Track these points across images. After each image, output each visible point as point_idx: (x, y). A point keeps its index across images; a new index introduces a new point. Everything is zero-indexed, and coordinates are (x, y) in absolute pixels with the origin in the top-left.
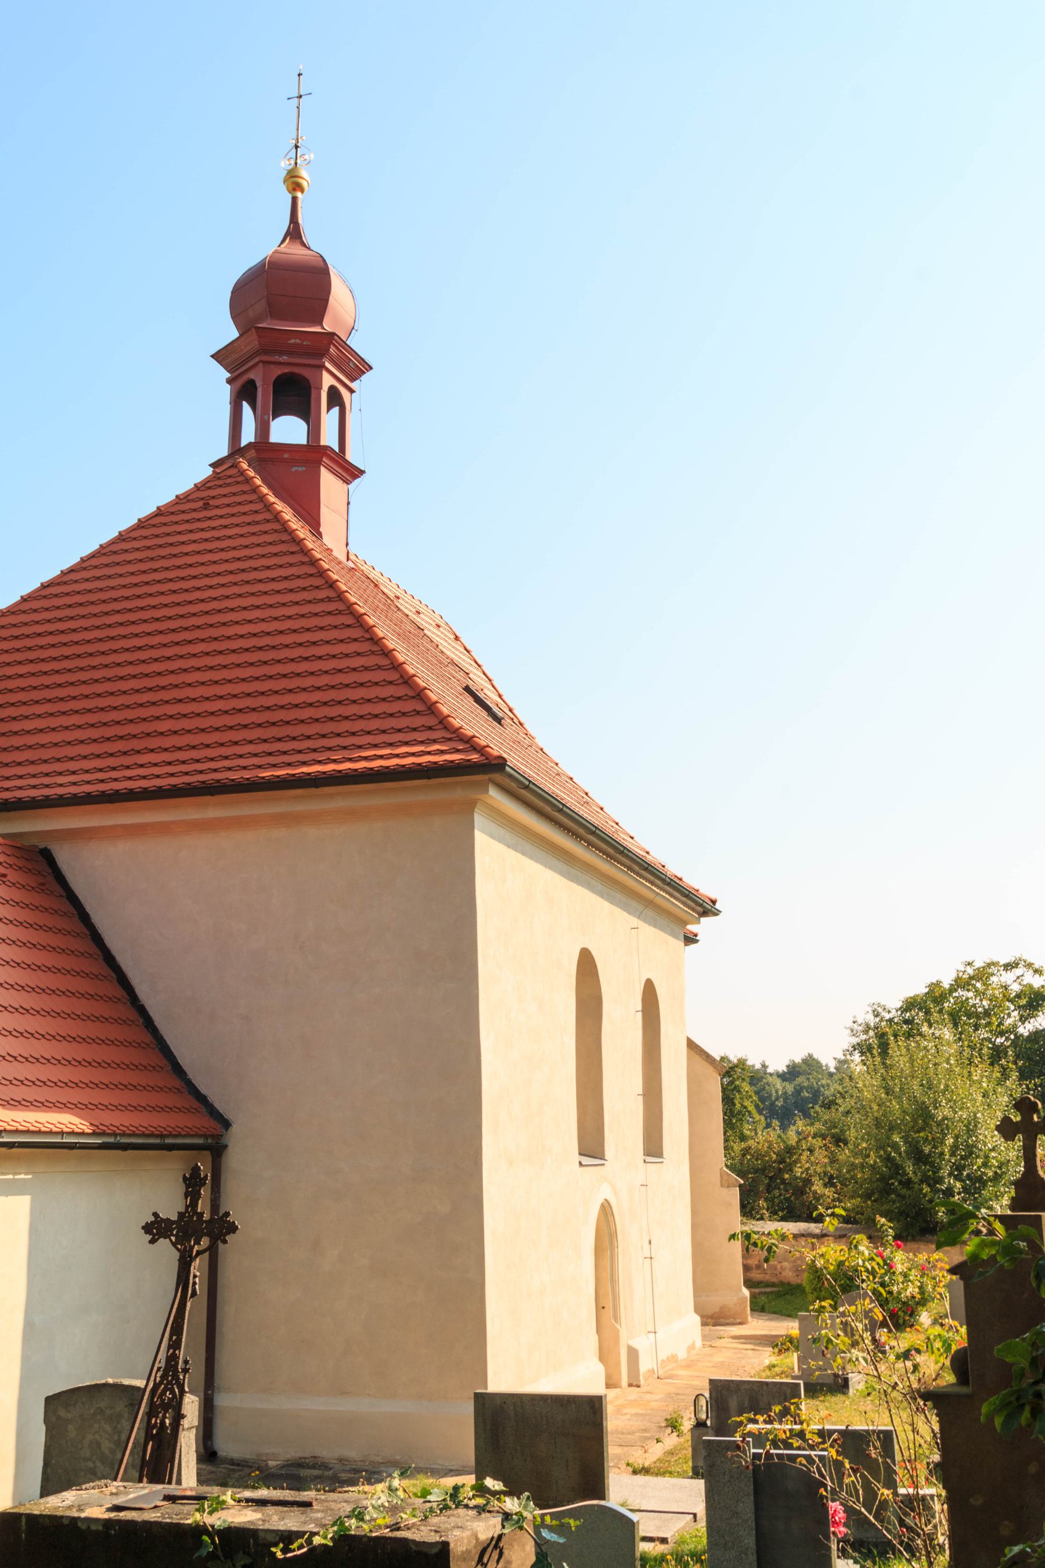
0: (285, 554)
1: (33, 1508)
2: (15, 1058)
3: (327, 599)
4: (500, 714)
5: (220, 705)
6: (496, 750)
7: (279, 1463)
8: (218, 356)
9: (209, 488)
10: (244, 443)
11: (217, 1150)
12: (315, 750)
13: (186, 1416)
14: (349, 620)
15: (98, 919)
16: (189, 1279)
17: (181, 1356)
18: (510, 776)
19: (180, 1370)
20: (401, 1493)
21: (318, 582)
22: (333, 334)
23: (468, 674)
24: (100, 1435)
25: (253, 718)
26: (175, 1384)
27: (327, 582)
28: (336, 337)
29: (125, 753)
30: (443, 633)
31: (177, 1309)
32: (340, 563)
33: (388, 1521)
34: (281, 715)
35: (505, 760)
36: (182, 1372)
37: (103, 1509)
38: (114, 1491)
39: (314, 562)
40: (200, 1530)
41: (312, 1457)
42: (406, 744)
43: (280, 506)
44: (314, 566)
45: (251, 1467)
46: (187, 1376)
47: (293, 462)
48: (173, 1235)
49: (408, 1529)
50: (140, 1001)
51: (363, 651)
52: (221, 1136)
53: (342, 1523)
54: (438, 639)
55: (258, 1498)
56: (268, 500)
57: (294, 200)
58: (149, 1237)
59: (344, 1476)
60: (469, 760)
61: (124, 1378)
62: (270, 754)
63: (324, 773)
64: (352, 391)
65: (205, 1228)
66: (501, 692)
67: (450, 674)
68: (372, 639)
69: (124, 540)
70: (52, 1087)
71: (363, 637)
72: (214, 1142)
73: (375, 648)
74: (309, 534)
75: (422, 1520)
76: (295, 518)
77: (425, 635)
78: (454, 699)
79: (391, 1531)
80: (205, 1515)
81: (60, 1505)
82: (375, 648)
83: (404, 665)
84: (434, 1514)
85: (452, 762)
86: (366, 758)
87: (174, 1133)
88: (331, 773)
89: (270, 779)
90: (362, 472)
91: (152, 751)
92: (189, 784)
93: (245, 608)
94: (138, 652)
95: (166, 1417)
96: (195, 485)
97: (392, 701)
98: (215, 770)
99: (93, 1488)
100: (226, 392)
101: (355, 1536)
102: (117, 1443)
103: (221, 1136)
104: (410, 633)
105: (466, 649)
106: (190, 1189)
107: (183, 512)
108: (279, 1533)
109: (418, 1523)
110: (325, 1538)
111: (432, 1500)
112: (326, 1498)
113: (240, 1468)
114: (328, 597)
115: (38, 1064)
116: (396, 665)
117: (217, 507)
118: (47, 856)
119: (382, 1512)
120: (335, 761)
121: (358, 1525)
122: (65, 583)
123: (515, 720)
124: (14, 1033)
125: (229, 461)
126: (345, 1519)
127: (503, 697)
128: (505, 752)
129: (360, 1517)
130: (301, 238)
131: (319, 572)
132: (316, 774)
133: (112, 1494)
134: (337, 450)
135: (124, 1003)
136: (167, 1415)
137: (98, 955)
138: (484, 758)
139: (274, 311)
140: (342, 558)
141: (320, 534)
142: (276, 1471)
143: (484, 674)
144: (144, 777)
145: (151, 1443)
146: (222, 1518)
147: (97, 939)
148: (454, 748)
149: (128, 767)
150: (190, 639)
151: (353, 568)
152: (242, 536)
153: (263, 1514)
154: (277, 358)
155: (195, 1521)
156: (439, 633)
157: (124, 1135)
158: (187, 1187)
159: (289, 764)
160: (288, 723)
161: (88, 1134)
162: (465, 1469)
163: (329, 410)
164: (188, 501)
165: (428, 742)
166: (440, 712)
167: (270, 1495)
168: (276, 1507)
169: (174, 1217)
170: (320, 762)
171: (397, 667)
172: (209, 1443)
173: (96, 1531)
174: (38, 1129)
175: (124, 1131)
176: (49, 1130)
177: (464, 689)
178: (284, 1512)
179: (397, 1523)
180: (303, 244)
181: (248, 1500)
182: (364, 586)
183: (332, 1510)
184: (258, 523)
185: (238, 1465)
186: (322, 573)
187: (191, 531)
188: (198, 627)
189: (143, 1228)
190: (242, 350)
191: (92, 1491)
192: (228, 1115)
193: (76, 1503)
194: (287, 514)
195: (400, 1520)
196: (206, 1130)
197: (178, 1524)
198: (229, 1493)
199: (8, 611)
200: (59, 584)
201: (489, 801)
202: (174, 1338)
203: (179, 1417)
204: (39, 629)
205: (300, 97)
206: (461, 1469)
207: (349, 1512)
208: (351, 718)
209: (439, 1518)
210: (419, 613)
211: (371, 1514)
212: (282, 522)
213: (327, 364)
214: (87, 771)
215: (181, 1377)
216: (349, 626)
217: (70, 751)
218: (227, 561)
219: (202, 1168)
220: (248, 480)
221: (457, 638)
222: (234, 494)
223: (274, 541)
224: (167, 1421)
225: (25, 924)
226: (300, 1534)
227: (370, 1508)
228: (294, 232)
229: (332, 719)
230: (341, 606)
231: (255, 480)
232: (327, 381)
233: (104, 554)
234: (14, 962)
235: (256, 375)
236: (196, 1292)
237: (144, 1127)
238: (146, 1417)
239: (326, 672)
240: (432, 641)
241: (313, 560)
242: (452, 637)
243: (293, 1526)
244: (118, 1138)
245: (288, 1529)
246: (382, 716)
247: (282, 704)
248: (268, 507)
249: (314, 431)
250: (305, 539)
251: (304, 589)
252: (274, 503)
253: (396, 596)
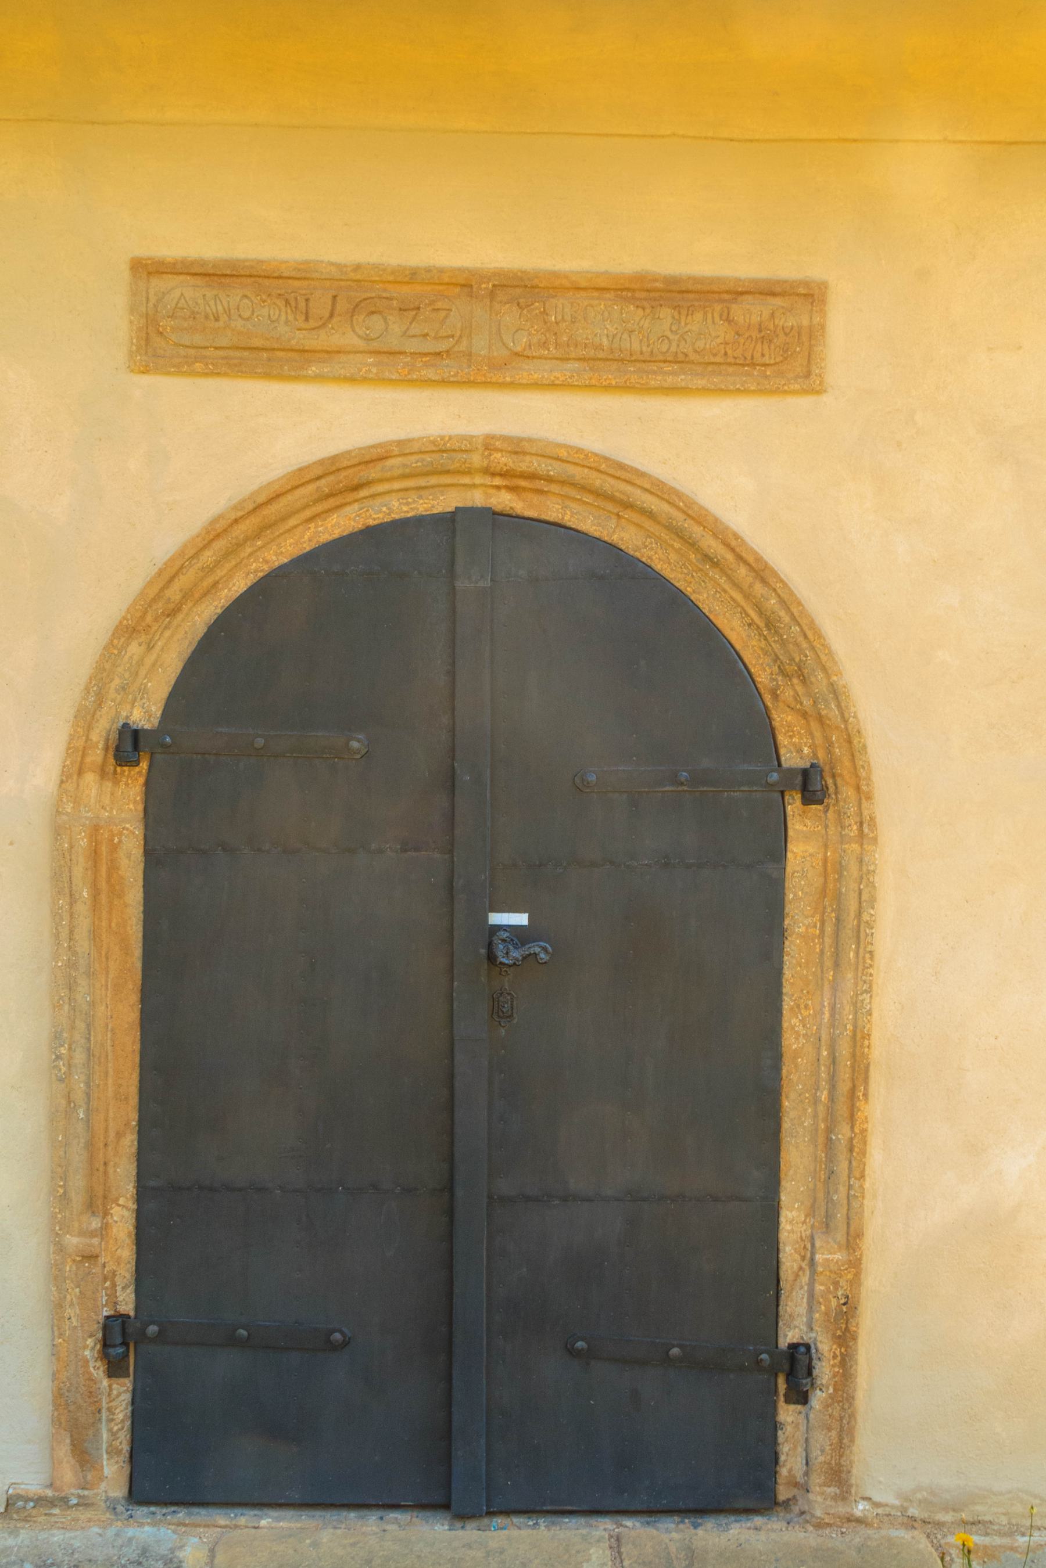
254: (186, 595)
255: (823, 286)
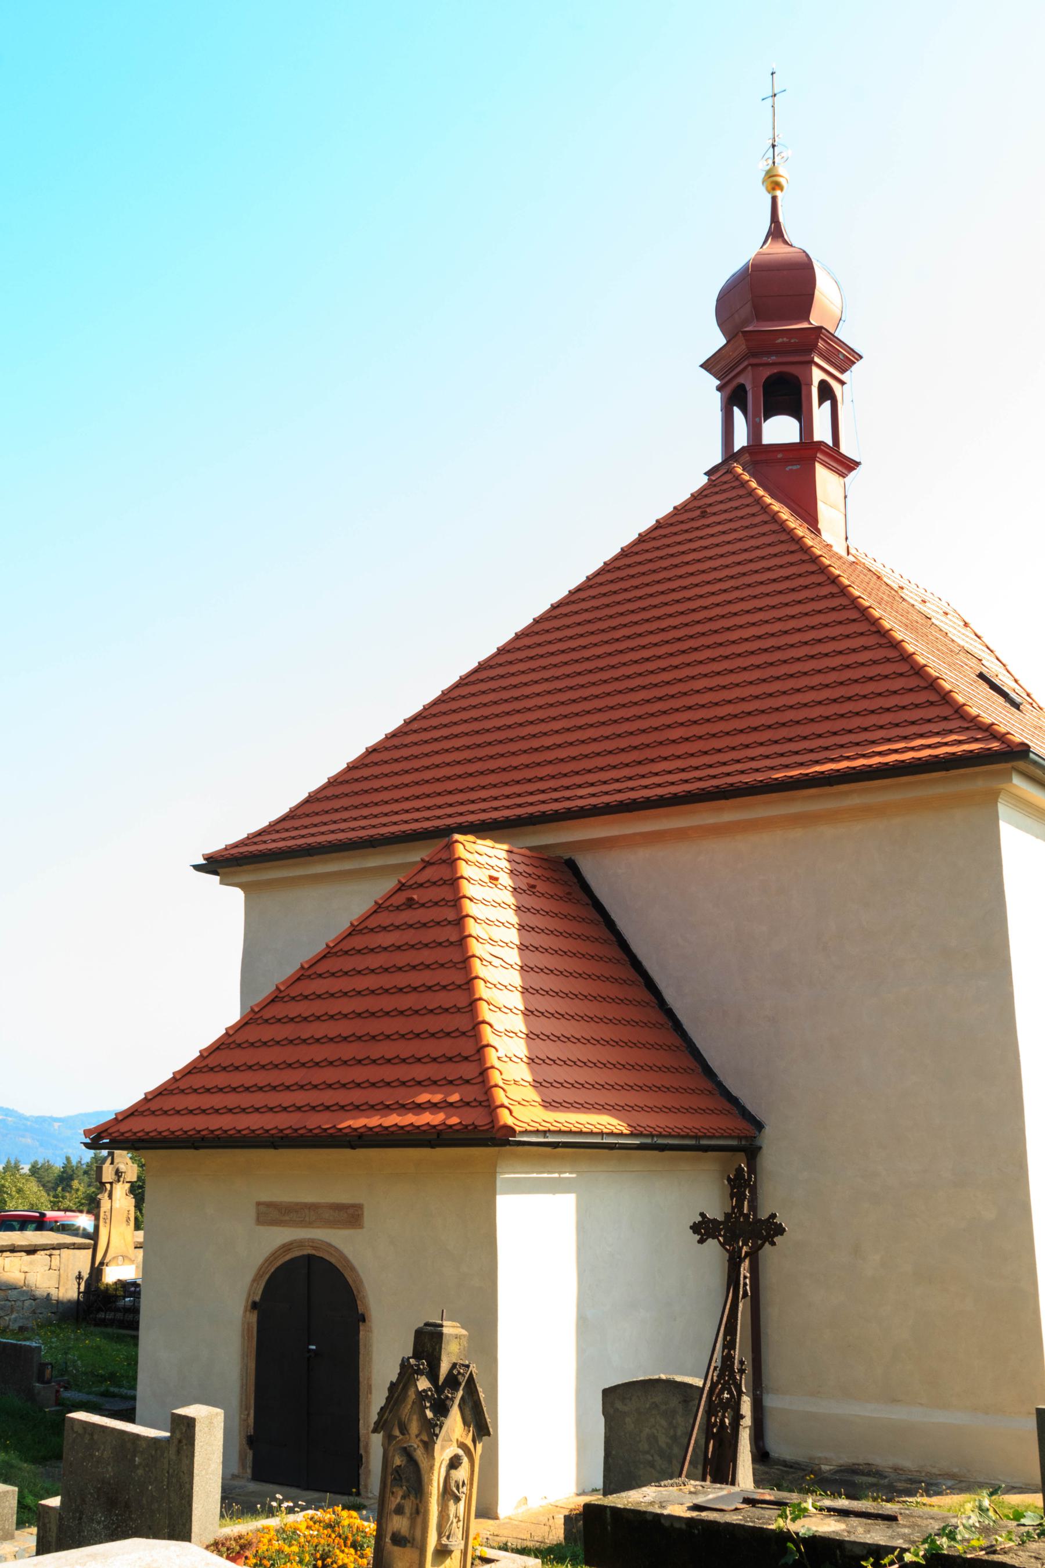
0: (785, 554)
1: (616, 1501)
2: (554, 1061)
3: (830, 596)
4: (1018, 700)
5: (729, 709)
6: (1018, 738)
7: (832, 1467)
8: (707, 366)
9: (706, 496)
10: (737, 448)
11: (752, 1152)
12: (827, 748)
13: (745, 1417)
14: (854, 615)
15: (622, 925)
16: (740, 1280)
17: (737, 1356)
18: (1035, 763)
19: (736, 1371)
20: (991, 1513)
21: (821, 578)
22: (821, 328)
23: (980, 660)
24: (657, 1429)
25: (763, 720)
26: (721, 1384)
27: (829, 578)
28: (823, 331)
29: (640, 763)
30: (951, 620)
31: (729, 1309)
32: (840, 558)
33: (984, 1543)
34: (791, 715)
35: (1028, 747)
36: (738, 1372)
37: (685, 1507)
38: (693, 1489)
39: (815, 559)
40: (784, 1536)
41: (865, 1464)
42: (922, 736)
43: (776, 506)
44: (816, 563)
45: (804, 1470)
46: (743, 1377)
47: (787, 461)
48: (721, 1236)
49: (1005, 1553)
50: (667, 1005)
51: (869, 645)
52: (755, 1137)
53: (933, 1542)
54: (946, 627)
55: (840, 1508)
56: (764, 502)
57: (774, 199)
58: (698, 1237)
59: (900, 1485)
60: (989, 749)
61: (676, 1374)
62: (782, 755)
63: (838, 771)
64: (842, 383)
65: (722, 1229)
66: (1016, 677)
67: (962, 662)
68: (878, 632)
69: (626, 555)
70: (569, 1088)
71: (869, 630)
72: (748, 1143)
73: (883, 641)
74: (807, 532)
75: (1019, 1544)
76: (793, 518)
77: (933, 623)
78: (968, 687)
79: (987, 1553)
80: (788, 1521)
81: (642, 1500)
82: (883, 641)
83: (914, 656)
84: (1032, 1539)
85: (971, 751)
86: (880, 754)
87: (709, 1134)
88: (844, 770)
89: (783, 780)
90: (858, 464)
91: (665, 759)
92: (703, 789)
93: (748, 612)
94: (646, 663)
95: (725, 1417)
96: (692, 495)
97: (873, 698)
98: (728, 774)
99: (672, 1485)
100: (715, 400)
101: (948, 1556)
102: (674, 1438)
103: (755, 1137)
104: (917, 622)
105: (976, 635)
106: (735, 1190)
107: (682, 522)
108: (867, 1546)
109: (1016, 1548)
110: (917, 1555)
111: (1026, 1524)
112: (911, 1513)
113: (792, 1470)
114: (831, 593)
115: (575, 1067)
116: (905, 656)
117: (714, 514)
118: (571, 865)
119: (974, 1533)
120: (848, 758)
121: (949, 1544)
122: (573, 602)
123: (1034, 705)
124: (552, 1037)
125: (724, 467)
126: (936, 1537)
127: (1019, 682)
128: (1026, 738)
129: (952, 1536)
130: (782, 236)
131: (820, 568)
132: (829, 772)
133: (691, 1493)
134: (831, 444)
135: (653, 1007)
136: (727, 1415)
137: (625, 960)
138: (1006, 746)
139: (761, 312)
140: (843, 553)
141: (819, 531)
142: (829, 1476)
143: (998, 659)
144: (659, 785)
145: (712, 1442)
146: (806, 1526)
147: (623, 944)
148: (972, 738)
149: (643, 776)
150: (696, 646)
151: (854, 562)
152: (740, 540)
153: (847, 1525)
154: (765, 359)
155: (779, 1527)
156: (947, 621)
157: (660, 1135)
158: (732, 1188)
159: (802, 764)
160: (798, 722)
161: (626, 1135)
162: (1028, 1487)
163: (820, 403)
164: (686, 511)
165: (943, 732)
166: (955, 701)
167: (851, 1506)
168: (860, 1519)
169: (720, 1218)
170: (832, 760)
171: (907, 658)
172: (761, 1443)
173: (680, 1529)
174: (579, 1130)
175: (661, 1133)
176: (610, 1131)
177: (977, 676)
178: (869, 1524)
179: (993, 1546)
180: (786, 242)
181: (829, 1509)
182: (867, 579)
183: (919, 1526)
184: (755, 526)
185: (791, 1467)
186: (824, 570)
187: (690, 540)
188: (703, 634)
189: (691, 1228)
190: (730, 356)
191: (671, 1488)
192: (760, 1116)
193: (657, 1500)
194: (785, 514)
195: (994, 1543)
196: (739, 1132)
197: (762, 1528)
198: (810, 1501)
199: (523, 634)
200: (567, 604)
201: (1014, 791)
202: (728, 1338)
203: (738, 1417)
204: (552, 648)
205: (775, 95)
206: (1024, 1487)
207: (939, 1530)
208: (862, 713)
209: (1038, 1544)
210: (925, 602)
211: (962, 1533)
212: (780, 523)
213: (817, 359)
214: (605, 783)
215: (738, 1378)
216: (854, 620)
217: (450, 786)
218: (727, 566)
219: (746, 1169)
220: (744, 484)
221: (966, 625)
222: (730, 500)
223: (773, 542)
224: (727, 1421)
225: (564, 934)
226: (891, 1550)
227: (961, 1528)
228: (776, 232)
229: (842, 716)
230: (845, 602)
231: (751, 483)
232: (817, 375)
233: (609, 571)
234: (548, 969)
235: (746, 380)
236: (747, 1293)
237: (722, 1129)
238: (705, 1415)
239: (834, 669)
240: (941, 630)
241: (814, 558)
242: (962, 624)
243: (881, 1540)
244: (655, 1139)
245: (875, 1543)
246: (894, 709)
247: (791, 704)
248: (766, 508)
249: (807, 428)
250: (804, 537)
251: (806, 587)
252: (771, 504)
253: (900, 587)
254: (263, 1273)
255: (363, 1205)
